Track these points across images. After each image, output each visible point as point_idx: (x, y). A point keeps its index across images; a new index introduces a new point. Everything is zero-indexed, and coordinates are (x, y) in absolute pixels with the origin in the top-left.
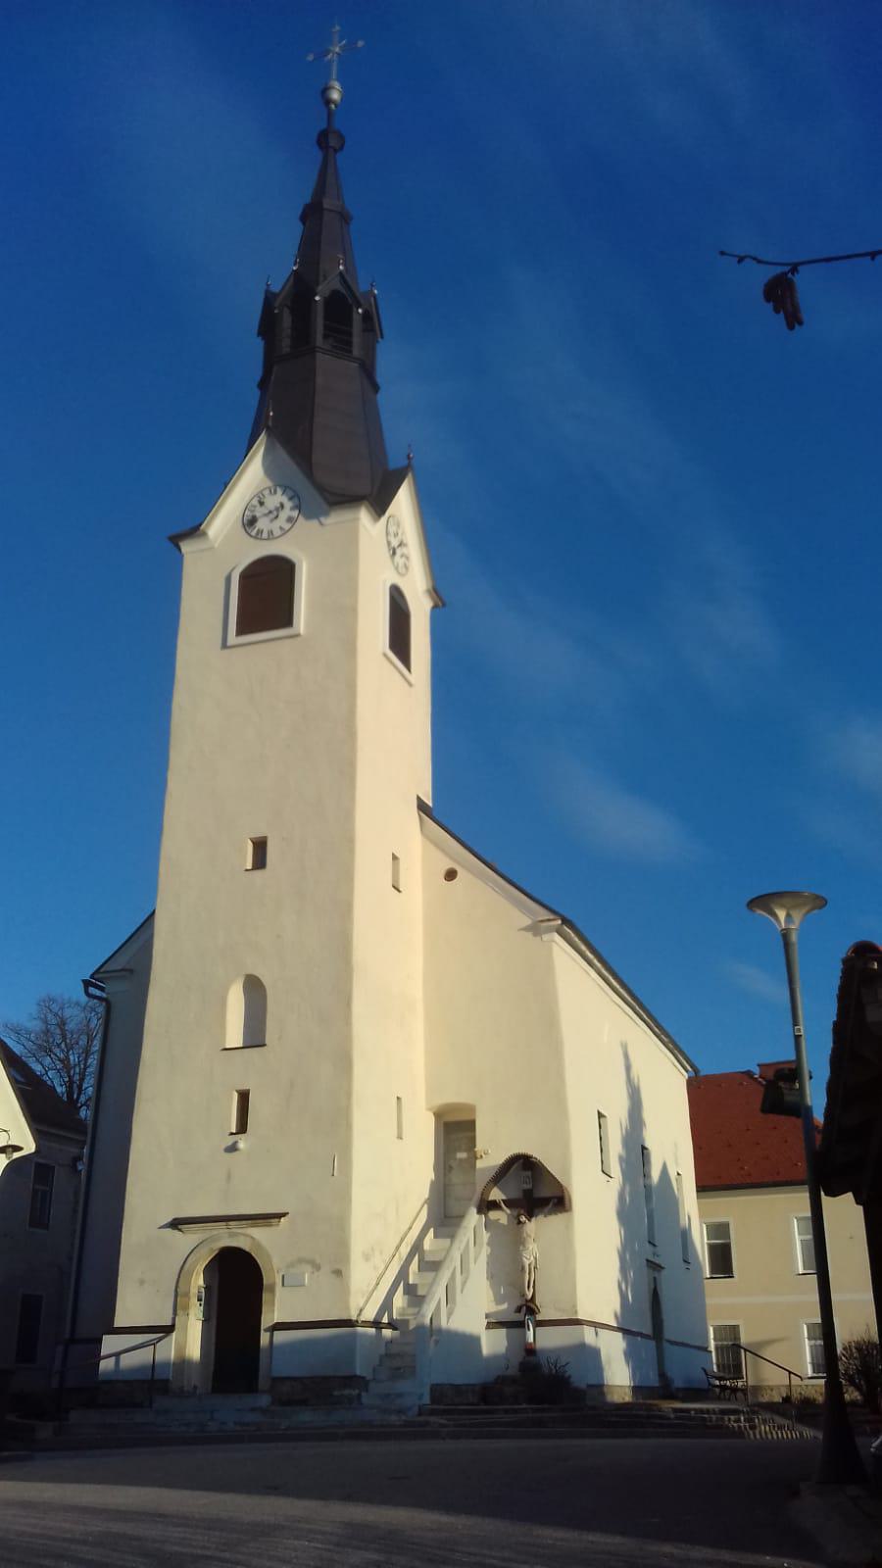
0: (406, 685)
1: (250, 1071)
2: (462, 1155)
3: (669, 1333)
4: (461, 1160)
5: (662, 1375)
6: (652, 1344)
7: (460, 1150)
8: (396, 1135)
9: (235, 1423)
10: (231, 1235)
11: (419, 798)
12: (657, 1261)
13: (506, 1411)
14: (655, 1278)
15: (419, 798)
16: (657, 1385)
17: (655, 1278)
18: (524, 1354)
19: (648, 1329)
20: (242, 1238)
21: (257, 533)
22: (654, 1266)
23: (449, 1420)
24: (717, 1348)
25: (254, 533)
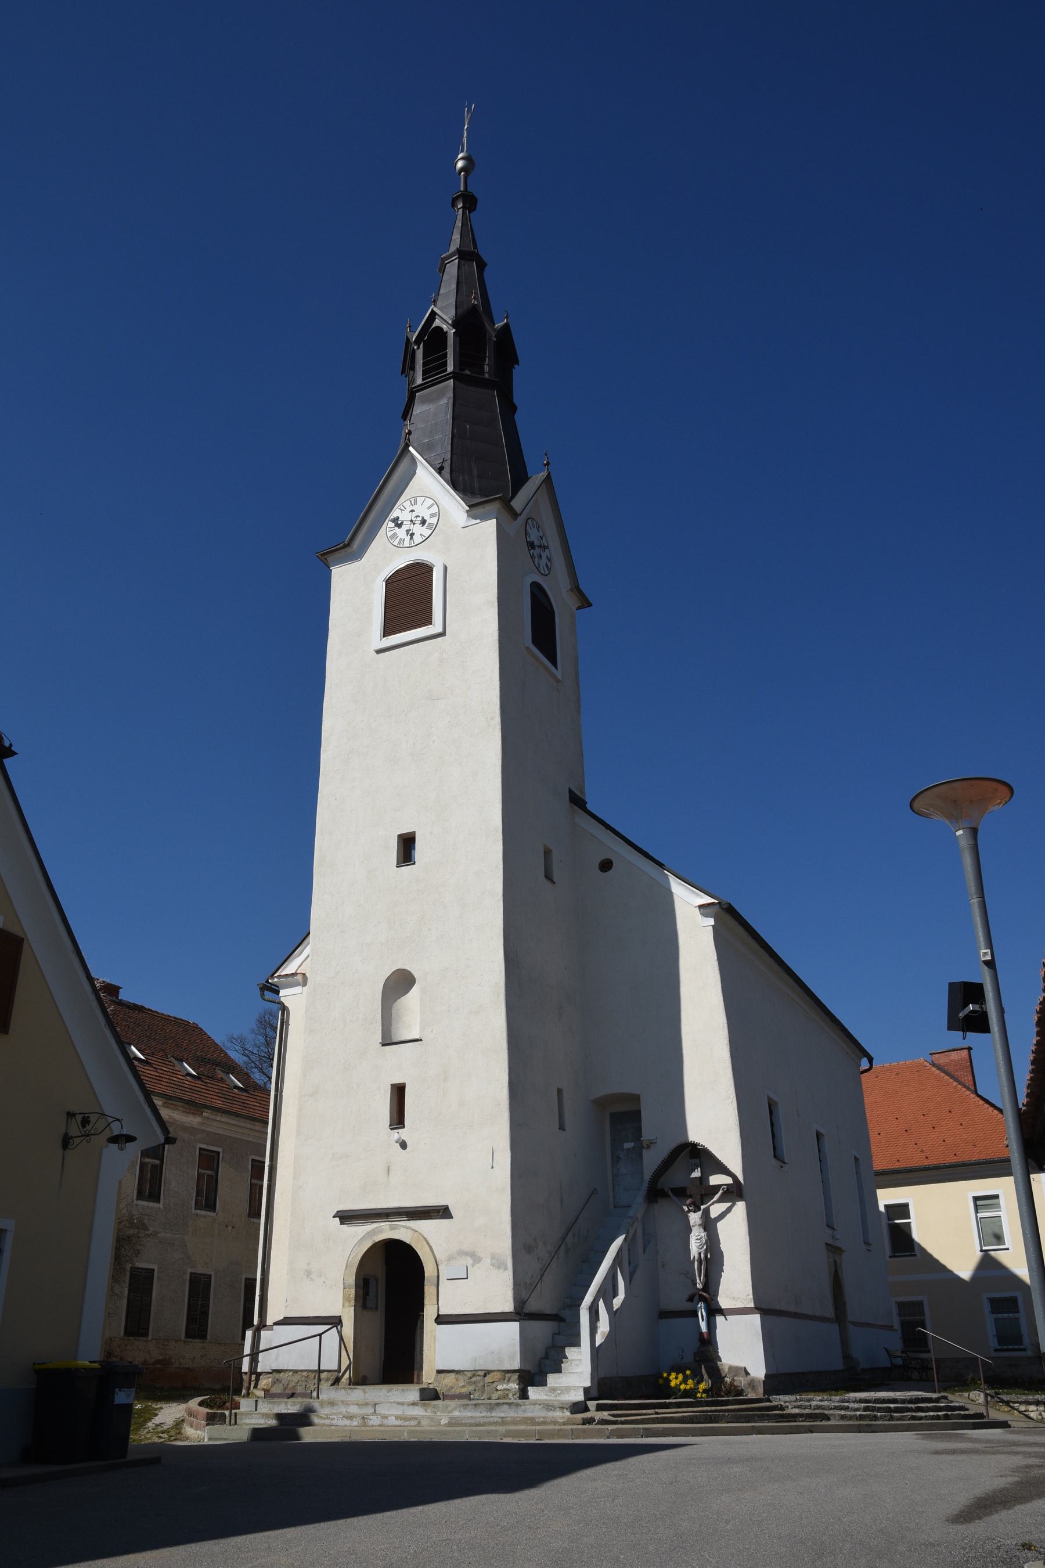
0: (781, 1112)
1: (398, 1066)
2: (628, 1145)
3: (854, 1312)
4: (628, 1149)
5: (847, 1357)
6: (835, 1327)
7: (627, 1141)
8: (379, 1039)
9: (397, 1417)
10: (392, 1228)
11: (570, 791)
12: (838, 1244)
13: (679, 1405)
14: (835, 1262)
15: (570, 791)
16: (842, 1368)
17: (835, 1262)
18: (698, 1344)
19: (829, 1312)
20: (403, 1230)
21: (399, 543)
22: (834, 1250)
23: (613, 1415)
24: (940, 1392)
25: (396, 543)
